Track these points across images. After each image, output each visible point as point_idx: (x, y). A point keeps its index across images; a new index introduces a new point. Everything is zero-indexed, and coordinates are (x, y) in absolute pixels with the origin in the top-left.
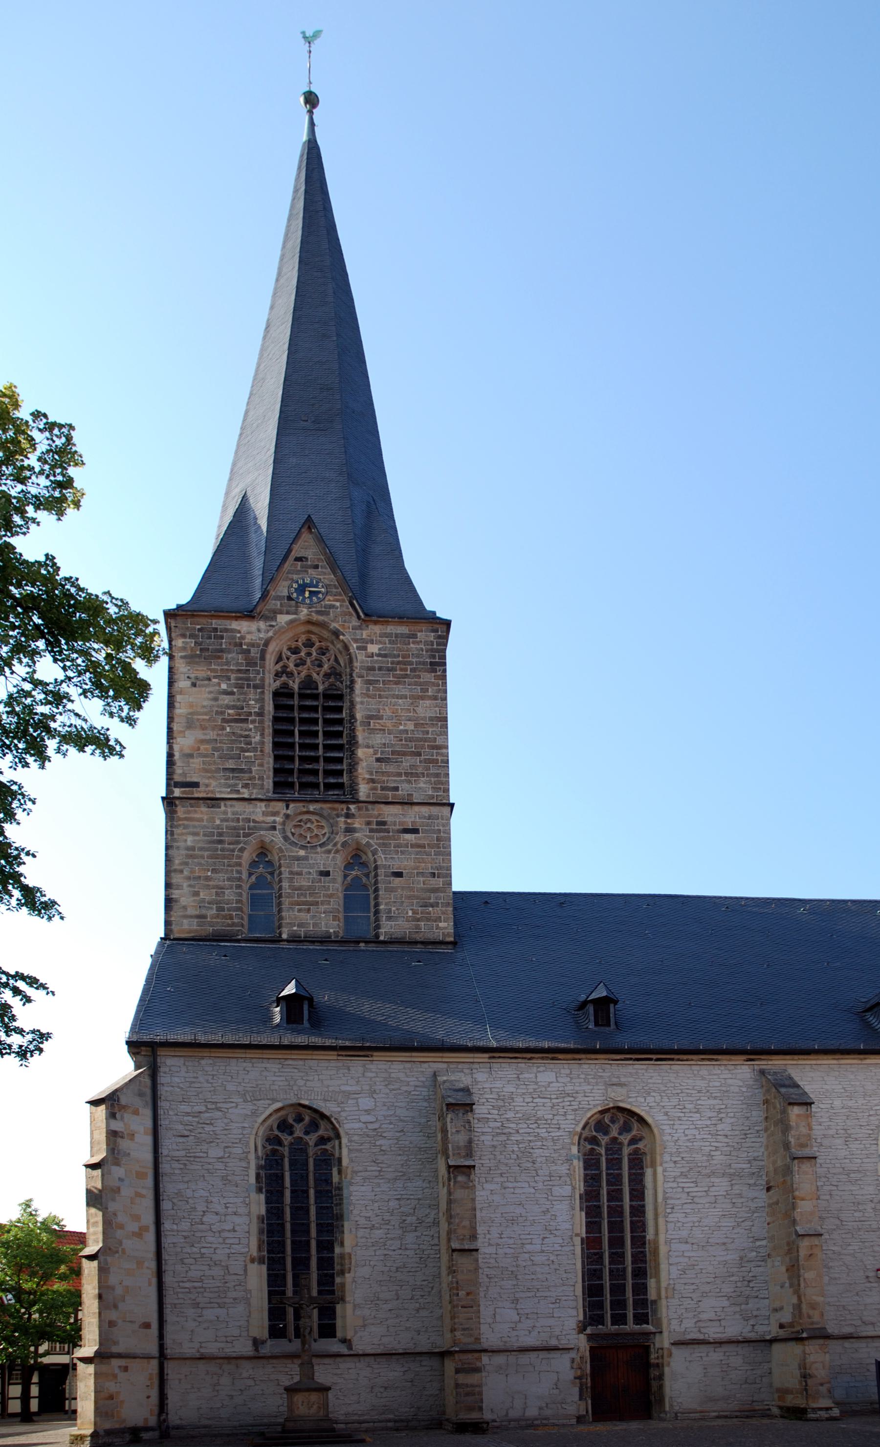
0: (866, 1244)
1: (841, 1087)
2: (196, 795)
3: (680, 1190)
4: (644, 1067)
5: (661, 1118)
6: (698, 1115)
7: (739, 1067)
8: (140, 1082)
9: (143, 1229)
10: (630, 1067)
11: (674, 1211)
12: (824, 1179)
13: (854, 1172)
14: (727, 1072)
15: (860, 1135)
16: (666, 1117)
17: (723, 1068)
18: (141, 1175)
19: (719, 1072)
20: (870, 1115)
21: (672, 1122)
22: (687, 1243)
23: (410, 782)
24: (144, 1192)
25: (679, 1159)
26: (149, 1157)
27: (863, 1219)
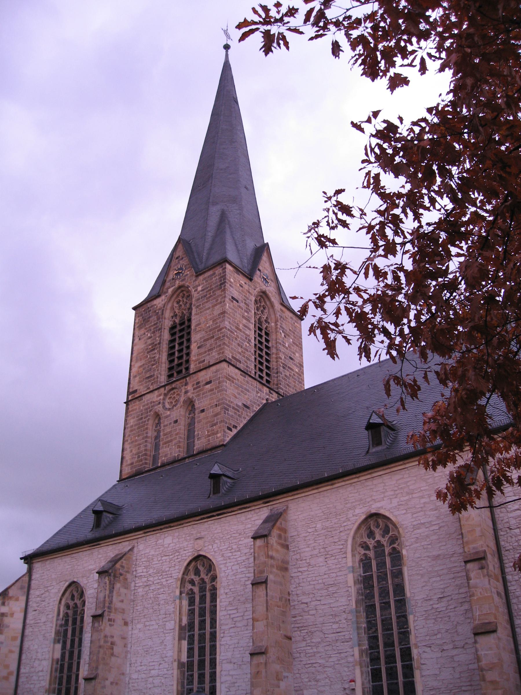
0: (342, 655)
1: (321, 511)
2: (136, 396)
3: (228, 616)
4: (213, 522)
5: (219, 559)
6: (239, 553)
7: (261, 509)
8: (23, 580)
9: (10, 673)
10: (206, 524)
11: (225, 635)
12: (311, 596)
13: (332, 585)
14: (256, 515)
15: (335, 551)
16: (222, 558)
17: (253, 512)
18: (14, 639)
19: (251, 516)
20: (341, 532)
21: (225, 562)
22: (231, 662)
23: (209, 354)
24: (14, 649)
25: (228, 591)
26: (20, 626)
27: (338, 630)
